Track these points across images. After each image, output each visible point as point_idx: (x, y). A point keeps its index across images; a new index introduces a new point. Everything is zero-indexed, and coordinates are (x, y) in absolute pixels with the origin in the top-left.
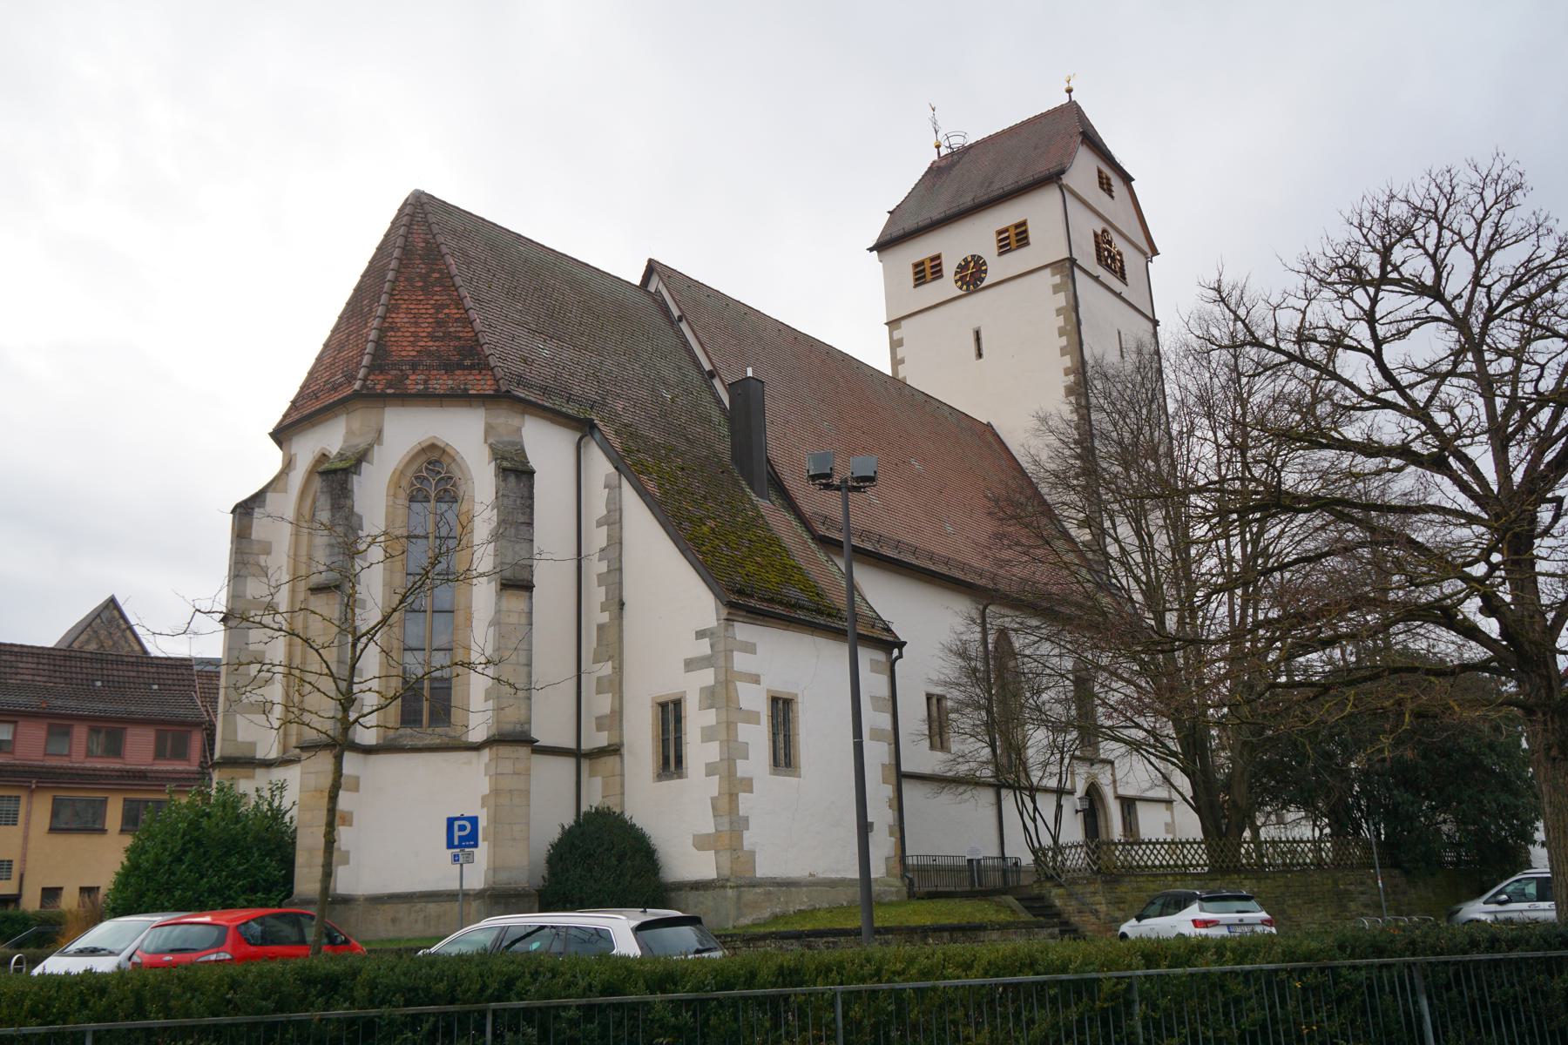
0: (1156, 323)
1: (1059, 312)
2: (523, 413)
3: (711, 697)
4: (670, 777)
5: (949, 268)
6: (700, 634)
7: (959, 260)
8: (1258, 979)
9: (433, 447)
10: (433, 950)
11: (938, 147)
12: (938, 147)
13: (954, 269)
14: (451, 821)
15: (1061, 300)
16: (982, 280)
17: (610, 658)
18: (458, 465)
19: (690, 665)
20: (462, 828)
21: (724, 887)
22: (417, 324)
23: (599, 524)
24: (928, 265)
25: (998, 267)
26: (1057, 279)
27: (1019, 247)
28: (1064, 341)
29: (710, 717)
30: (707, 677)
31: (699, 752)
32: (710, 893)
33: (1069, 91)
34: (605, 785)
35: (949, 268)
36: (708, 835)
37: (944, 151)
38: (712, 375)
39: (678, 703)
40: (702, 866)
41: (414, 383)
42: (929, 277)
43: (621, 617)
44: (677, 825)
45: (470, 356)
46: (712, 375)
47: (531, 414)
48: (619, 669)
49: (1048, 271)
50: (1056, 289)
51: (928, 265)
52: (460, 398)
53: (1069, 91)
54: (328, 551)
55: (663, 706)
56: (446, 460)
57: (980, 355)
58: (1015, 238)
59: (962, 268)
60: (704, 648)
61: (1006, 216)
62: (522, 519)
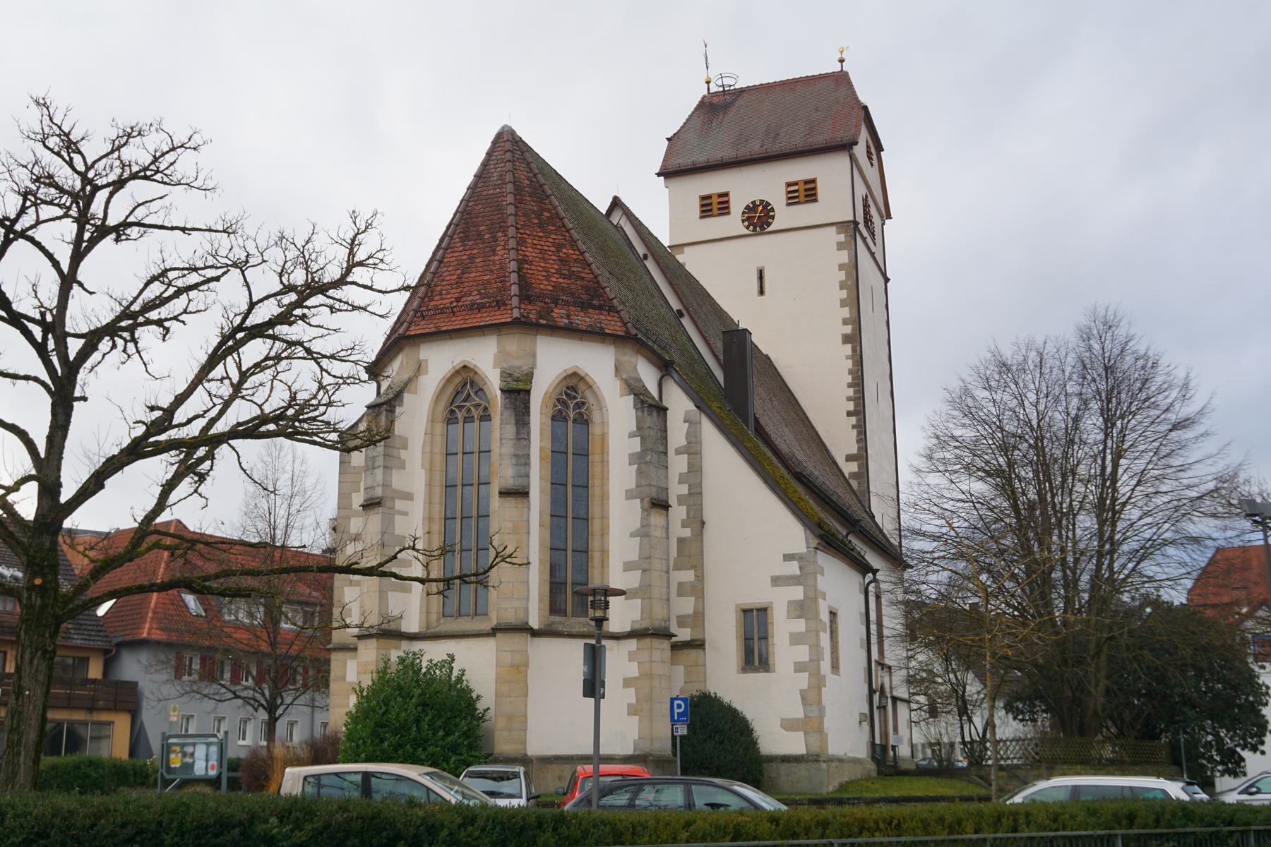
0: (887, 280)
1: (841, 267)
2: (638, 352)
3: (802, 609)
4: (756, 670)
5: (738, 206)
6: (788, 557)
7: (748, 201)
8: (1102, 840)
9: (575, 374)
10: (1018, 799)
11: (708, 83)
12: (708, 83)
13: (742, 209)
14: (673, 700)
15: (844, 257)
17: (693, 567)
18: (594, 393)
19: (777, 581)
20: (679, 706)
21: (818, 761)
22: (545, 260)
23: (678, 452)
24: (715, 200)
25: (784, 216)
26: (842, 238)
27: (807, 202)
28: (844, 294)
29: (800, 625)
30: (797, 593)
31: (785, 649)
32: (803, 766)
33: (842, 61)
34: (687, 674)
35: (738, 206)
36: (798, 720)
37: (714, 89)
38: (680, 314)
39: (763, 610)
40: (794, 744)
41: (559, 314)
42: (715, 211)
43: (701, 535)
44: (772, 711)
45: (594, 298)
46: (680, 314)
47: (645, 357)
48: (700, 578)
49: (834, 229)
50: (840, 246)
51: (715, 200)
52: (596, 335)
53: (842, 61)
54: (514, 461)
55: (746, 612)
56: (582, 387)
57: (762, 292)
58: (805, 193)
59: (751, 208)
60: (793, 568)
61: (799, 170)
62: (661, 449)
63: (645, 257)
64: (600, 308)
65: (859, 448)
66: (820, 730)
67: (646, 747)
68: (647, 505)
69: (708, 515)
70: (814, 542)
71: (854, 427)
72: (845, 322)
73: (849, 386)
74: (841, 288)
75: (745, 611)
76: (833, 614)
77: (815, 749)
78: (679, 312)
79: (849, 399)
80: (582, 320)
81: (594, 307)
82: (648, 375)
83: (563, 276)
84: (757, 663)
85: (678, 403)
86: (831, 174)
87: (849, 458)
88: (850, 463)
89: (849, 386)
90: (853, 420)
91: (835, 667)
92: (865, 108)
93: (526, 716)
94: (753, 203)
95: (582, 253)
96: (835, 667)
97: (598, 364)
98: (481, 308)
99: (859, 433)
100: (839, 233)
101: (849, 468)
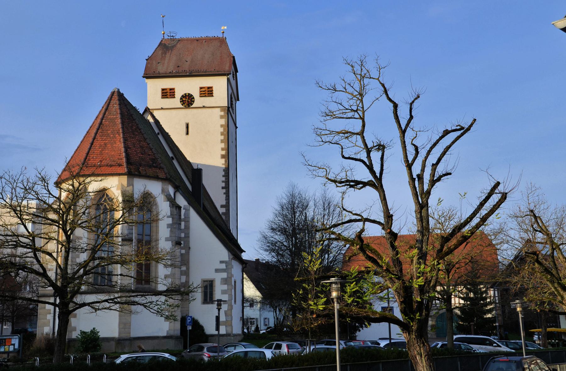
0: (236, 128)
1: (222, 126)
2: (169, 183)
3: (225, 281)
4: (208, 303)
5: (178, 95)
6: (222, 262)
7: (183, 93)
16: (192, 104)
17: (185, 265)
19: (217, 271)
25: (199, 101)
26: (222, 113)
28: (222, 137)
29: (225, 287)
30: (224, 275)
35: (178, 95)
37: (166, 37)
46: (172, 158)
48: (188, 269)
49: (219, 109)
50: (222, 117)
52: (156, 178)
57: (187, 133)
58: (208, 92)
60: (223, 266)
61: (206, 82)
63: (158, 134)
64: (156, 167)
65: (226, 203)
66: (231, 326)
67: (172, 333)
68: (174, 244)
69: (191, 245)
70: (232, 257)
71: (224, 193)
72: (222, 149)
73: (223, 176)
74: (222, 135)
75: (204, 281)
76: (235, 282)
77: (229, 332)
78: (172, 157)
79: (223, 182)
80: (150, 172)
81: (154, 167)
82: (171, 190)
83: (142, 154)
84: (208, 300)
85: (181, 201)
86: (220, 84)
87: (222, 206)
88: (222, 209)
89: (223, 176)
90: (224, 191)
91: (235, 301)
92: (234, 57)
93: (130, 323)
94: (185, 94)
95: (148, 144)
96: (235, 301)
97: (155, 188)
98: (111, 166)
99: (226, 196)
100: (221, 111)
101: (222, 211)
